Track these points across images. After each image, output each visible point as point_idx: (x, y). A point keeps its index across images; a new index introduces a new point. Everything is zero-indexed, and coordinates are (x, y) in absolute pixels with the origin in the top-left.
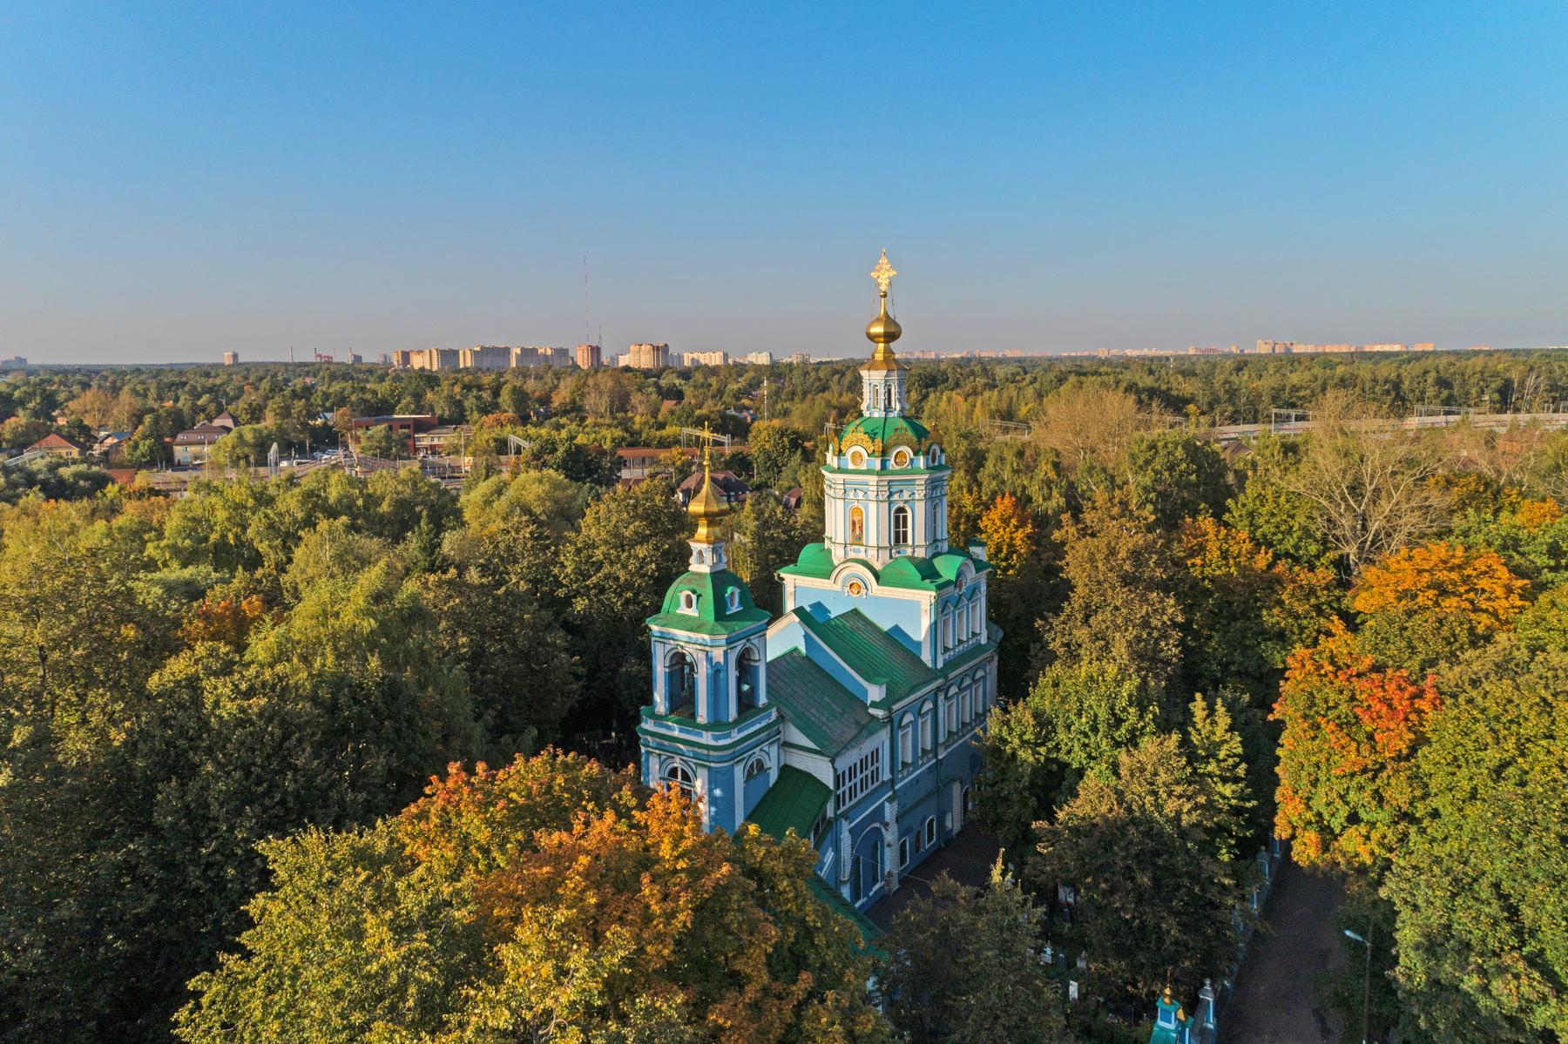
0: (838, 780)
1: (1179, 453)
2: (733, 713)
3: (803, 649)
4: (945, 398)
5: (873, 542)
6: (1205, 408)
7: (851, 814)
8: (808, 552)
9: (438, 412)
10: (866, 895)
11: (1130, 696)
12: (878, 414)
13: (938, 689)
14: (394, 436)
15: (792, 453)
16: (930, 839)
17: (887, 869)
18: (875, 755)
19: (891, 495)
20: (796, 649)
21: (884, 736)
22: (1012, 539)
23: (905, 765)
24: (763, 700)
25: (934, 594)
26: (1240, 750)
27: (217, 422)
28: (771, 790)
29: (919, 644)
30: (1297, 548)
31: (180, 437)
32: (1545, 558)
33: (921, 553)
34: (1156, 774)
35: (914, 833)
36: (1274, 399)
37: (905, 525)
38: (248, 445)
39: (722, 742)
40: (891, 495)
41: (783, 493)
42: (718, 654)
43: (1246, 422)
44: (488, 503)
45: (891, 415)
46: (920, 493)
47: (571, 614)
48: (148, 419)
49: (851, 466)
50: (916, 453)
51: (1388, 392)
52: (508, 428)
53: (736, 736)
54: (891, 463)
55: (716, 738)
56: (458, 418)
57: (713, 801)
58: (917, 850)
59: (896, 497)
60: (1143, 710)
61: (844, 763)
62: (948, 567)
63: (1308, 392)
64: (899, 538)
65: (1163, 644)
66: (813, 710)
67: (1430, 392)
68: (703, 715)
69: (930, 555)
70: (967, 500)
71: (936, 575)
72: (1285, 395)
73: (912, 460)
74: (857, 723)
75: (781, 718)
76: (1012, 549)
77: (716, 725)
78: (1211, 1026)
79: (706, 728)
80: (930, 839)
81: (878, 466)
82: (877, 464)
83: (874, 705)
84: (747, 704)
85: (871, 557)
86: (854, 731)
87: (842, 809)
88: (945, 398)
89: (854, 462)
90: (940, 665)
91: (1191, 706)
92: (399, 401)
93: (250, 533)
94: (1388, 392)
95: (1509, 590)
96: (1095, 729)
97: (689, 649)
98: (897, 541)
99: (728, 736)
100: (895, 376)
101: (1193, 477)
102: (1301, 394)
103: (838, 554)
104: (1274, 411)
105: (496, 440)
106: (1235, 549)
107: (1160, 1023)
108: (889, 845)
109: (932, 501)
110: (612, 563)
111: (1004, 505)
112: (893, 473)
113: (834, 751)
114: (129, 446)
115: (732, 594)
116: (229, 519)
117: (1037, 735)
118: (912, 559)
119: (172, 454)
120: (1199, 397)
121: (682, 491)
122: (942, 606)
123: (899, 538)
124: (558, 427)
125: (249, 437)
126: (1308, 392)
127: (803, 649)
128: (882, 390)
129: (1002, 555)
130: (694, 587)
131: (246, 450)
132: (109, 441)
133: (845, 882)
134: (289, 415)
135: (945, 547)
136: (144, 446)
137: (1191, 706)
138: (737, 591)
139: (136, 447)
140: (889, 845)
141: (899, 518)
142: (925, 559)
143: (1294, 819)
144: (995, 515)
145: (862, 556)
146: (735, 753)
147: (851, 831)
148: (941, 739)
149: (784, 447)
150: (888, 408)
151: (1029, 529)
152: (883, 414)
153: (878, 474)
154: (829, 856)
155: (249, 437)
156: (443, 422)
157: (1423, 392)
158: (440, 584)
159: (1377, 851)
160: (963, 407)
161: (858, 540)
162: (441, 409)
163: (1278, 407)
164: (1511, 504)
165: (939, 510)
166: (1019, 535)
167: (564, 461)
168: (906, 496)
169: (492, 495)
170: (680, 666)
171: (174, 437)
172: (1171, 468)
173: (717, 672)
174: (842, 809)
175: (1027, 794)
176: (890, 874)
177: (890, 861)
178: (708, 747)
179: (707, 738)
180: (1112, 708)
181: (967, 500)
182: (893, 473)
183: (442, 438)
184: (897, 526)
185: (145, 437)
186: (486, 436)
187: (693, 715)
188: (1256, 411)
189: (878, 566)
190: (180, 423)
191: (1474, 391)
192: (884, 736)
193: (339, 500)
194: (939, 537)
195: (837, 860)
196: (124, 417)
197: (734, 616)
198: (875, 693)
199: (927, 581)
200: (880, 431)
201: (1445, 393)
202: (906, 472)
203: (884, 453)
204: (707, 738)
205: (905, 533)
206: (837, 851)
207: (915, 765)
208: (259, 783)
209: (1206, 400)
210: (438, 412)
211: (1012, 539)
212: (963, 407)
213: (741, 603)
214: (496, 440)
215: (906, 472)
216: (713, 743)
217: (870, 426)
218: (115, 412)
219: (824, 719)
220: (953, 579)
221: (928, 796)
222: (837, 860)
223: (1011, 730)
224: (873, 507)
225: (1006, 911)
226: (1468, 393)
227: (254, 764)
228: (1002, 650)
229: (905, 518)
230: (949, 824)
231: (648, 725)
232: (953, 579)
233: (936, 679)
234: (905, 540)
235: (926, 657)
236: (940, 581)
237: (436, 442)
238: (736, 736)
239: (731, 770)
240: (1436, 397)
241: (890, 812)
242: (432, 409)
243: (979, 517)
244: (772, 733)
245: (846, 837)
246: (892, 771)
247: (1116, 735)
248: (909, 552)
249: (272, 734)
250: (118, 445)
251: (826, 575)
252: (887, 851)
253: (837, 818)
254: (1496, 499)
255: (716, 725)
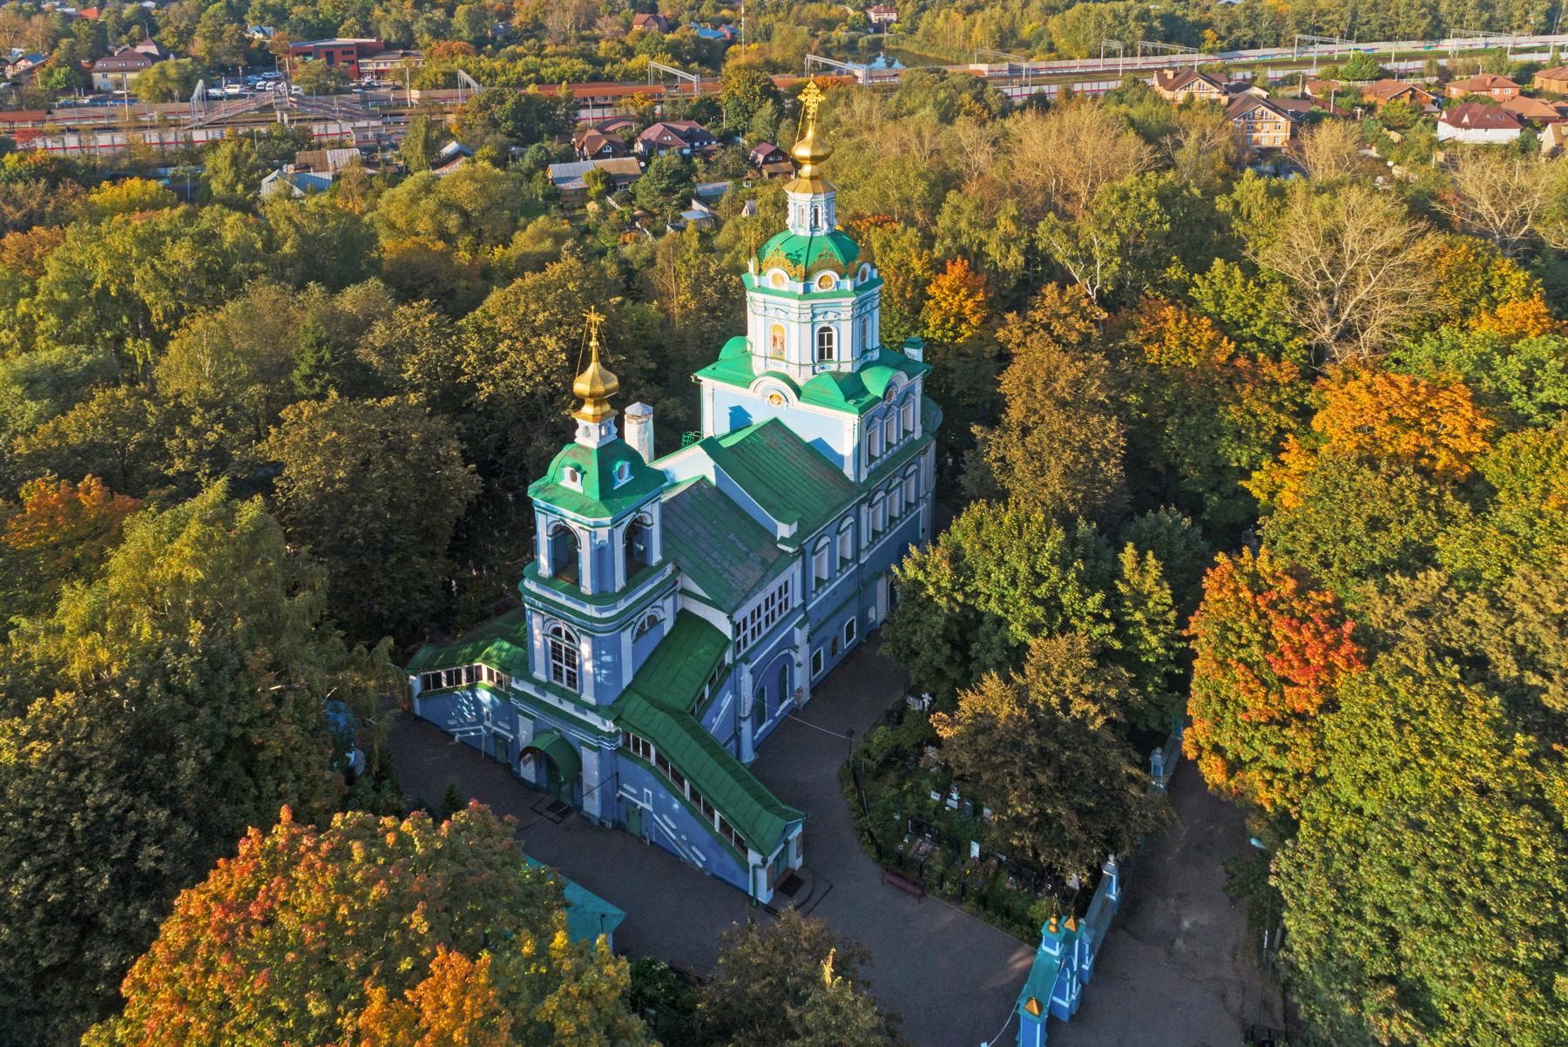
0: (737, 629)
1: (1153, 204)
2: (620, 582)
3: (712, 479)
4: (942, 16)
5: (794, 358)
6: (1223, 33)
7: (751, 657)
8: (729, 350)
9: (384, 36)
10: (771, 716)
11: (1053, 554)
12: (805, 232)
13: (862, 502)
14: (334, 70)
15: (763, 100)
16: (849, 637)
17: (797, 686)
18: (783, 589)
19: (814, 316)
20: (704, 478)
21: (796, 568)
22: (961, 307)
23: (820, 582)
24: (656, 557)
25: (856, 416)
26: (1170, 601)
27: (140, 49)
28: (665, 639)
29: (842, 457)
30: (1264, 331)
31: (99, 64)
32: (1517, 383)
33: (847, 368)
34: (1062, 674)
35: (829, 644)
36: (1298, 24)
37: (830, 342)
38: (173, 81)
39: (606, 615)
40: (814, 316)
41: (752, 146)
42: (603, 534)
43: (1266, 45)
44: (414, 200)
45: (817, 234)
46: (847, 313)
47: (475, 401)
48: (64, 42)
49: (772, 286)
50: (842, 277)
51: (1424, 16)
52: (460, 59)
53: (623, 605)
54: (815, 288)
55: (601, 611)
56: (406, 43)
57: (599, 666)
58: (834, 653)
59: (819, 318)
60: (1065, 566)
61: (742, 613)
62: (875, 382)
63: (1336, 16)
64: (824, 354)
65: (1103, 464)
66: (715, 554)
67: (1470, 16)
68: (587, 586)
69: (857, 368)
70: (916, 265)
71: (863, 391)
72: (1312, 20)
73: (838, 284)
74: (763, 562)
75: (678, 569)
76: (961, 319)
77: (602, 596)
78: (1113, 898)
79: (591, 600)
80: (849, 637)
81: (800, 290)
82: (799, 288)
83: (783, 540)
84: (637, 564)
85: (793, 373)
86: (759, 574)
87: (743, 651)
88: (942, 16)
89: (775, 282)
90: (864, 477)
91: (1121, 556)
92: (342, 22)
93: (136, 286)
94: (1424, 16)
95: (1473, 428)
96: (1014, 583)
97: (574, 526)
98: (821, 356)
99: (615, 607)
100: (822, 198)
101: (1167, 227)
102: (1328, 18)
103: (758, 365)
104: (1297, 36)
105: (444, 74)
106: (1195, 339)
107: (1044, 947)
108: (799, 665)
109: (860, 318)
110: (518, 351)
111: (957, 270)
112: (816, 296)
113: (733, 604)
114: (43, 74)
115: (622, 468)
116: (110, 271)
117: (953, 583)
118: (836, 376)
119: (91, 78)
120: (1217, 22)
121: (643, 142)
122: (867, 425)
123: (824, 354)
124: (514, 58)
125: (172, 72)
126: (1336, 16)
127: (712, 479)
128: (808, 211)
129: (949, 326)
130: (579, 462)
131: (169, 85)
132: (22, 64)
133: (745, 719)
134: (220, 39)
135: (876, 355)
136: (60, 74)
137: (1121, 556)
138: (627, 464)
139: (50, 74)
140: (799, 665)
141: (824, 340)
142: (851, 374)
143: (1202, 741)
144: (946, 281)
145: (783, 369)
146: (621, 622)
147: (752, 672)
148: (864, 544)
149: (755, 94)
150: (814, 227)
151: (980, 297)
152: (809, 234)
153: (800, 298)
154: (727, 700)
155: (172, 72)
156: (389, 47)
157: (1463, 15)
158: (316, 416)
159: (1278, 801)
160: (962, 25)
161: (779, 356)
162: (387, 32)
163: (1303, 32)
164: (1501, 276)
165: (869, 324)
166: (969, 304)
167: (514, 111)
168: (831, 316)
169: (419, 192)
170: (564, 539)
171: (93, 62)
172: (1142, 220)
173: (600, 553)
174: (743, 651)
175: (939, 641)
176: (800, 690)
177: (801, 678)
178: (591, 619)
179: (590, 610)
180: (1032, 567)
181: (916, 265)
182: (816, 296)
183: (393, 63)
184: (821, 342)
185: (60, 65)
186: (435, 69)
187: (577, 582)
188: (1279, 35)
189: (800, 382)
190: (100, 50)
191: (1517, 13)
192: (796, 568)
193: (235, 245)
194: (869, 346)
195: (736, 703)
196: (38, 38)
197: (627, 490)
198: (784, 530)
199: (851, 402)
200: (803, 259)
201: (1486, 16)
202: (831, 295)
203: (807, 276)
204: (590, 610)
205: (830, 351)
206: (736, 692)
207: (831, 580)
208: (41, 828)
209: (1225, 25)
210: (384, 36)
211: (961, 307)
212: (962, 25)
213: (631, 473)
214: (444, 74)
215: (831, 295)
216: (597, 615)
217: (791, 248)
218: (28, 33)
219: (726, 564)
220: (881, 395)
221: (848, 601)
222: (736, 703)
223: (927, 574)
224: (794, 327)
225: (836, 1010)
226: (1511, 15)
227: (36, 808)
228: (941, 436)
229: (830, 337)
230: (872, 614)
231: (529, 585)
232: (881, 395)
233: (861, 492)
234: (830, 355)
235: (849, 471)
236: (867, 399)
237: (382, 67)
238: (623, 605)
239: (618, 638)
240: (1476, 19)
241: (800, 636)
242: (378, 35)
243: (928, 282)
244: (669, 588)
245: (746, 680)
246: (804, 596)
247: (1036, 592)
248: (834, 367)
249: (56, 778)
250: (30, 71)
251: (747, 384)
252: (798, 672)
253: (736, 663)
254: (1486, 271)
255: (602, 596)
